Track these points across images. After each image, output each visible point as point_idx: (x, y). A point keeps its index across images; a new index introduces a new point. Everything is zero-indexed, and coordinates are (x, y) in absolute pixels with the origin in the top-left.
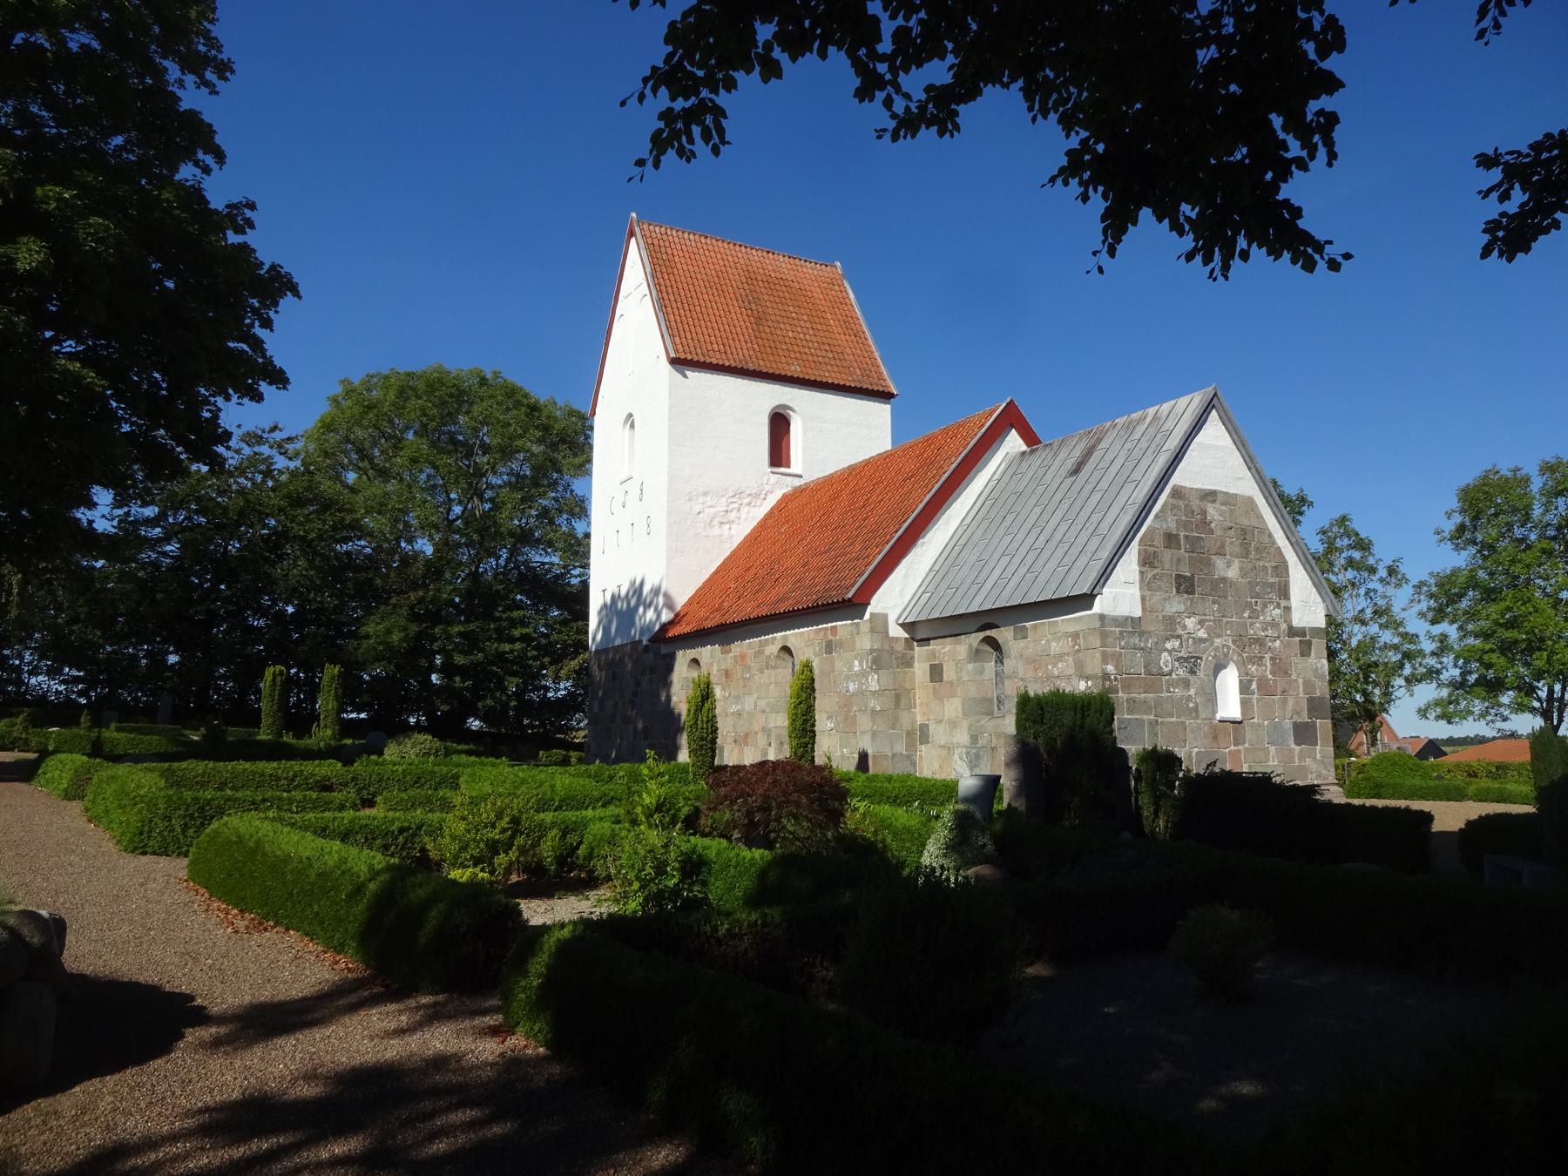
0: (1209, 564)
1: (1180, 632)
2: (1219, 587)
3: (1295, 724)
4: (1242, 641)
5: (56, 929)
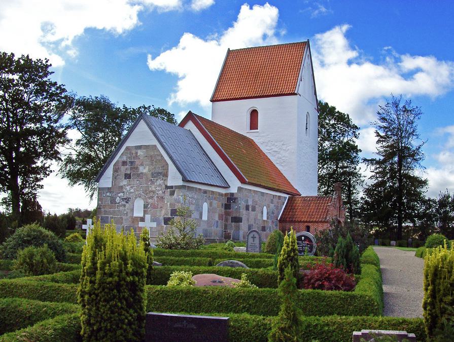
0: (137, 168)
1: (124, 190)
2: (140, 176)
3: (164, 218)
4: (146, 191)
5: (176, 48)
